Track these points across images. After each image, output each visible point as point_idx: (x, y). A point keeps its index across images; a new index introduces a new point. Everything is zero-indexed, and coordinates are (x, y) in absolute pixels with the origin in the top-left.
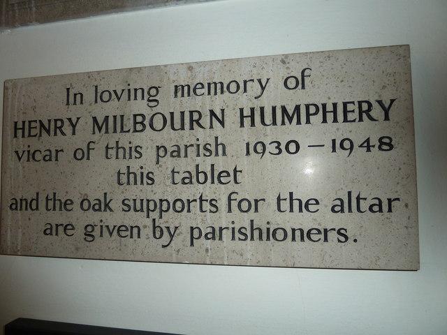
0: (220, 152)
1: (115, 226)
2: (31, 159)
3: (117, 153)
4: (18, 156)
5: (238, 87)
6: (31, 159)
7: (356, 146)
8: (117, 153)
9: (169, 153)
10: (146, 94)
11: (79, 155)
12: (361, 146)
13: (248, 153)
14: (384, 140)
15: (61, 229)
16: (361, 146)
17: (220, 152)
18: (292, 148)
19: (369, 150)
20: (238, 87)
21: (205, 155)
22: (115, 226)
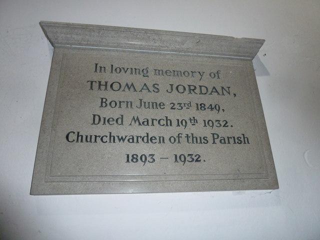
10: (141, 72)
11: (172, 139)
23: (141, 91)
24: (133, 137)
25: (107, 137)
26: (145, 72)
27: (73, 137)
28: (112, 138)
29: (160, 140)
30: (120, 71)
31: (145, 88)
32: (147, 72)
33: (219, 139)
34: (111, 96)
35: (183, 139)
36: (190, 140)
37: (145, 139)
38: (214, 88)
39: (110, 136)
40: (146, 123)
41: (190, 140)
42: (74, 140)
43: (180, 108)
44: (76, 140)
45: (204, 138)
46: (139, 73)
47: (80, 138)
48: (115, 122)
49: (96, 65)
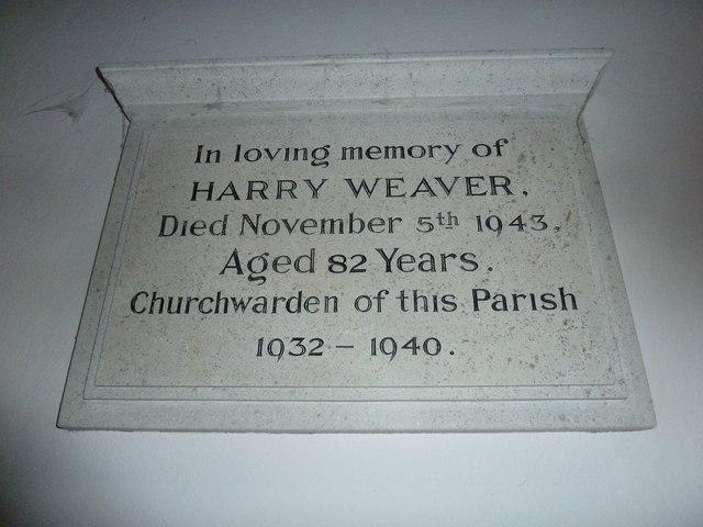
0: (453, 223)
1: (297, 221)
2: (378, 351)
3: (153, 304)
4: (354, 189)
5: (269, 348)
6: (378, 351)
7: (399, 346)
8: (153, 304)
9: (208, 226)
10: (309, 155)
11: (363, 304)
12: (405, 347)
13: (237, 159)
14: (336, 259)
15: (281, 305)
16: (405, 347)
17: (453, 223)
18: (432, 347)
19: (521, 228)
20: (269, 348)
21: (443, 309)
22: (297, 221)
23: (414, 195)
24: (504, 299)
25: (212, 300)
26: (320, 154)
27: (143, 302)
28: (222, 303)
29: (326, 305)
30: (260, 155)
31: (423, 187)
32: (327, 153)
33: (491, 301)
34: (268, 209)
35: (391, 302)
36: (409, 303)
37: (294, 303)
38: (231, 185)
39: (219, 300)
40: (427, 266)
41: (409, 303)
42: (144, 309)
43: (541, 226)
44: (148, 310)
45: (443, 300)
46: (305, 158)
47: (158, 303)
48: (292, 267)
49: (200, 147)
